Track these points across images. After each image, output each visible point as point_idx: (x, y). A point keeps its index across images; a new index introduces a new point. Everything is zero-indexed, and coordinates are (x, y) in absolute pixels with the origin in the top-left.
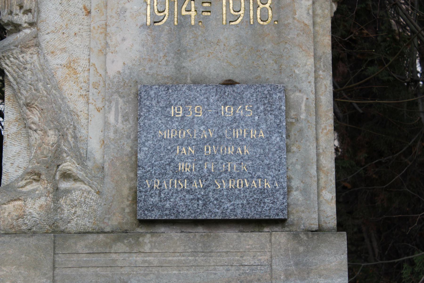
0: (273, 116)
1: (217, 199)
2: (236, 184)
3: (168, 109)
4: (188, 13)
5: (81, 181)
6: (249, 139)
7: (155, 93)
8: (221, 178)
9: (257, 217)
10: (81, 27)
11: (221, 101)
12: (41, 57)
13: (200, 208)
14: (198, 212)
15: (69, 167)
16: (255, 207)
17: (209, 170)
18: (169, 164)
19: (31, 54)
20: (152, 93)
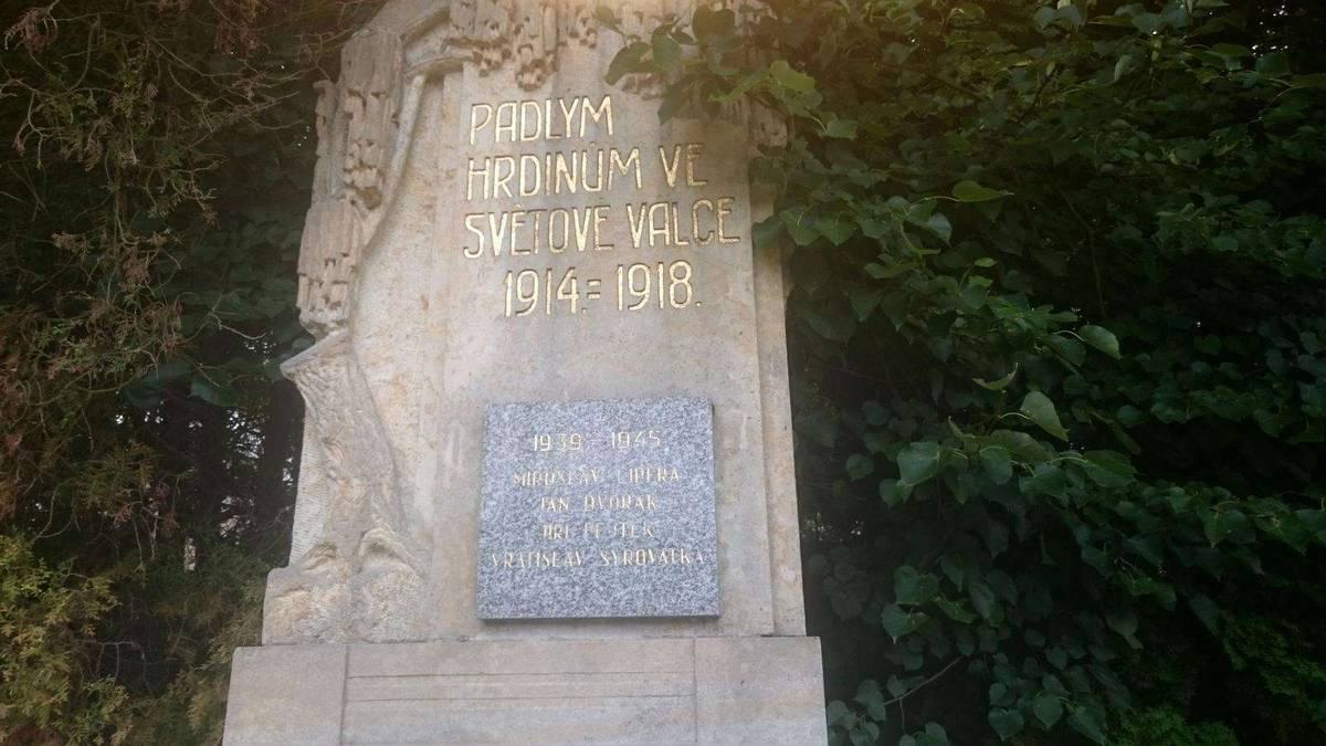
0: (693, 446)
1: (604, 584)
2: (635, 558)
3: (530, 440)
4: (566, 297)
5: (398, 557)
6: (655, 483)
7: (510, 416)
8: (612, 548)
9: (669, 613)
10: (416, 325)
11: (611, 424)
12: (354, 370)
13: (577, 598)
14: (572, 606)
15: (380, 536)
16: (665, 596)
17: (591, 535)
18: (529, 527)
19: (337, 365)
20: (506, 416)
